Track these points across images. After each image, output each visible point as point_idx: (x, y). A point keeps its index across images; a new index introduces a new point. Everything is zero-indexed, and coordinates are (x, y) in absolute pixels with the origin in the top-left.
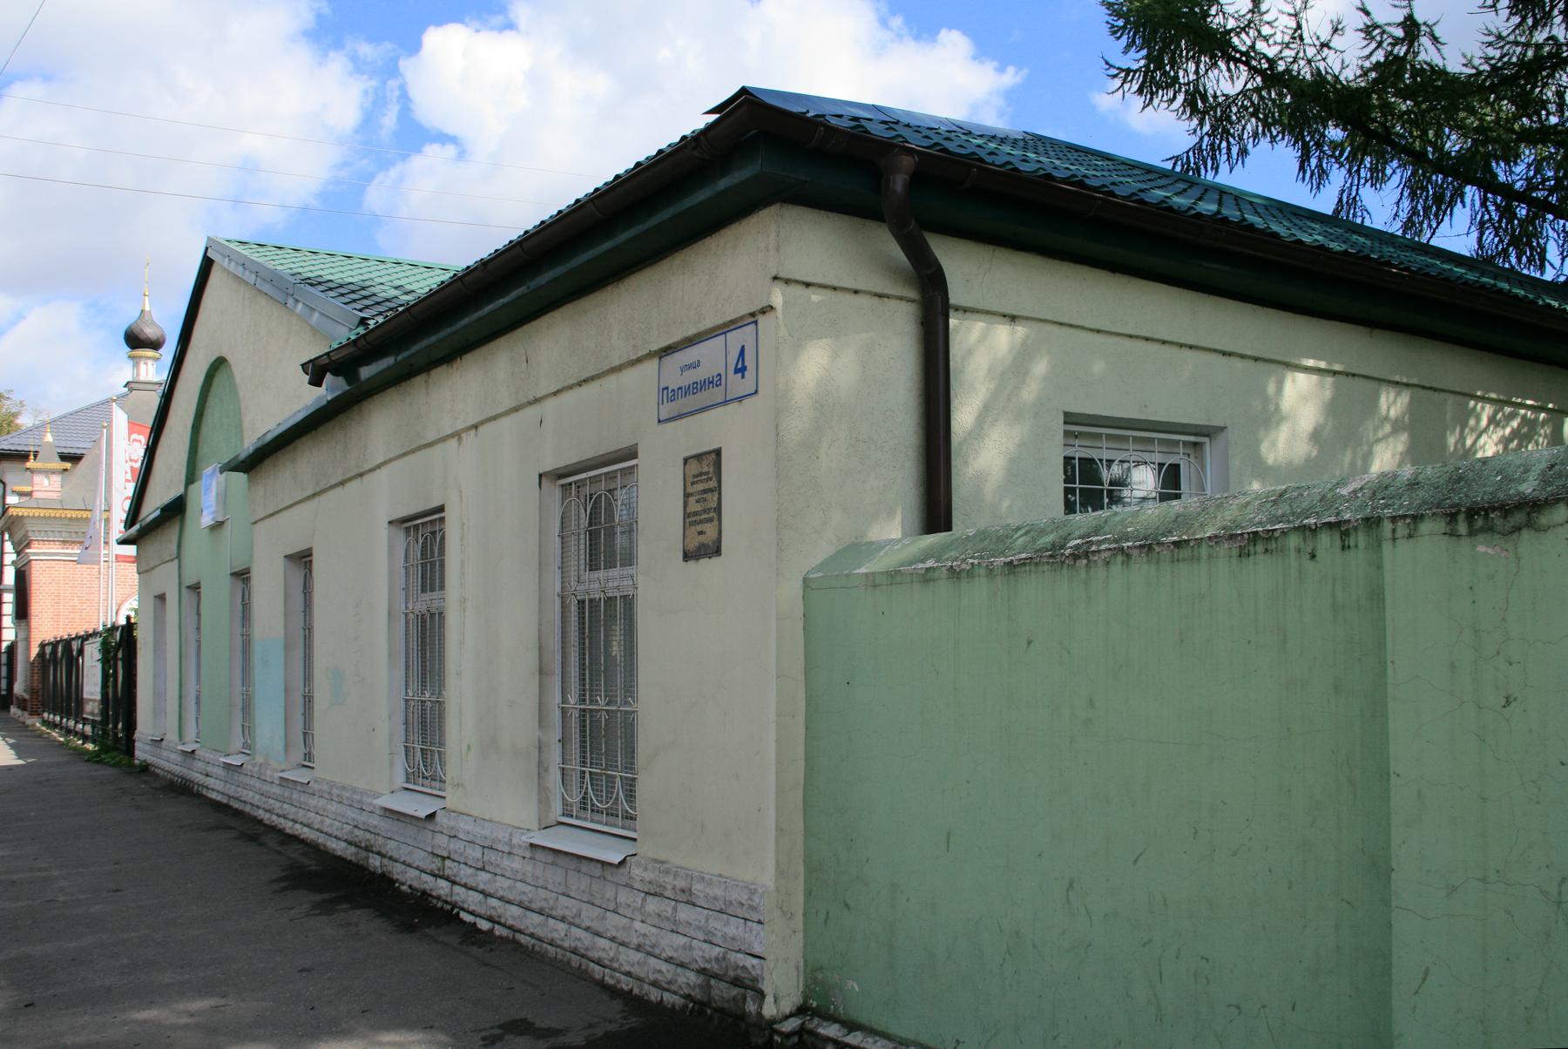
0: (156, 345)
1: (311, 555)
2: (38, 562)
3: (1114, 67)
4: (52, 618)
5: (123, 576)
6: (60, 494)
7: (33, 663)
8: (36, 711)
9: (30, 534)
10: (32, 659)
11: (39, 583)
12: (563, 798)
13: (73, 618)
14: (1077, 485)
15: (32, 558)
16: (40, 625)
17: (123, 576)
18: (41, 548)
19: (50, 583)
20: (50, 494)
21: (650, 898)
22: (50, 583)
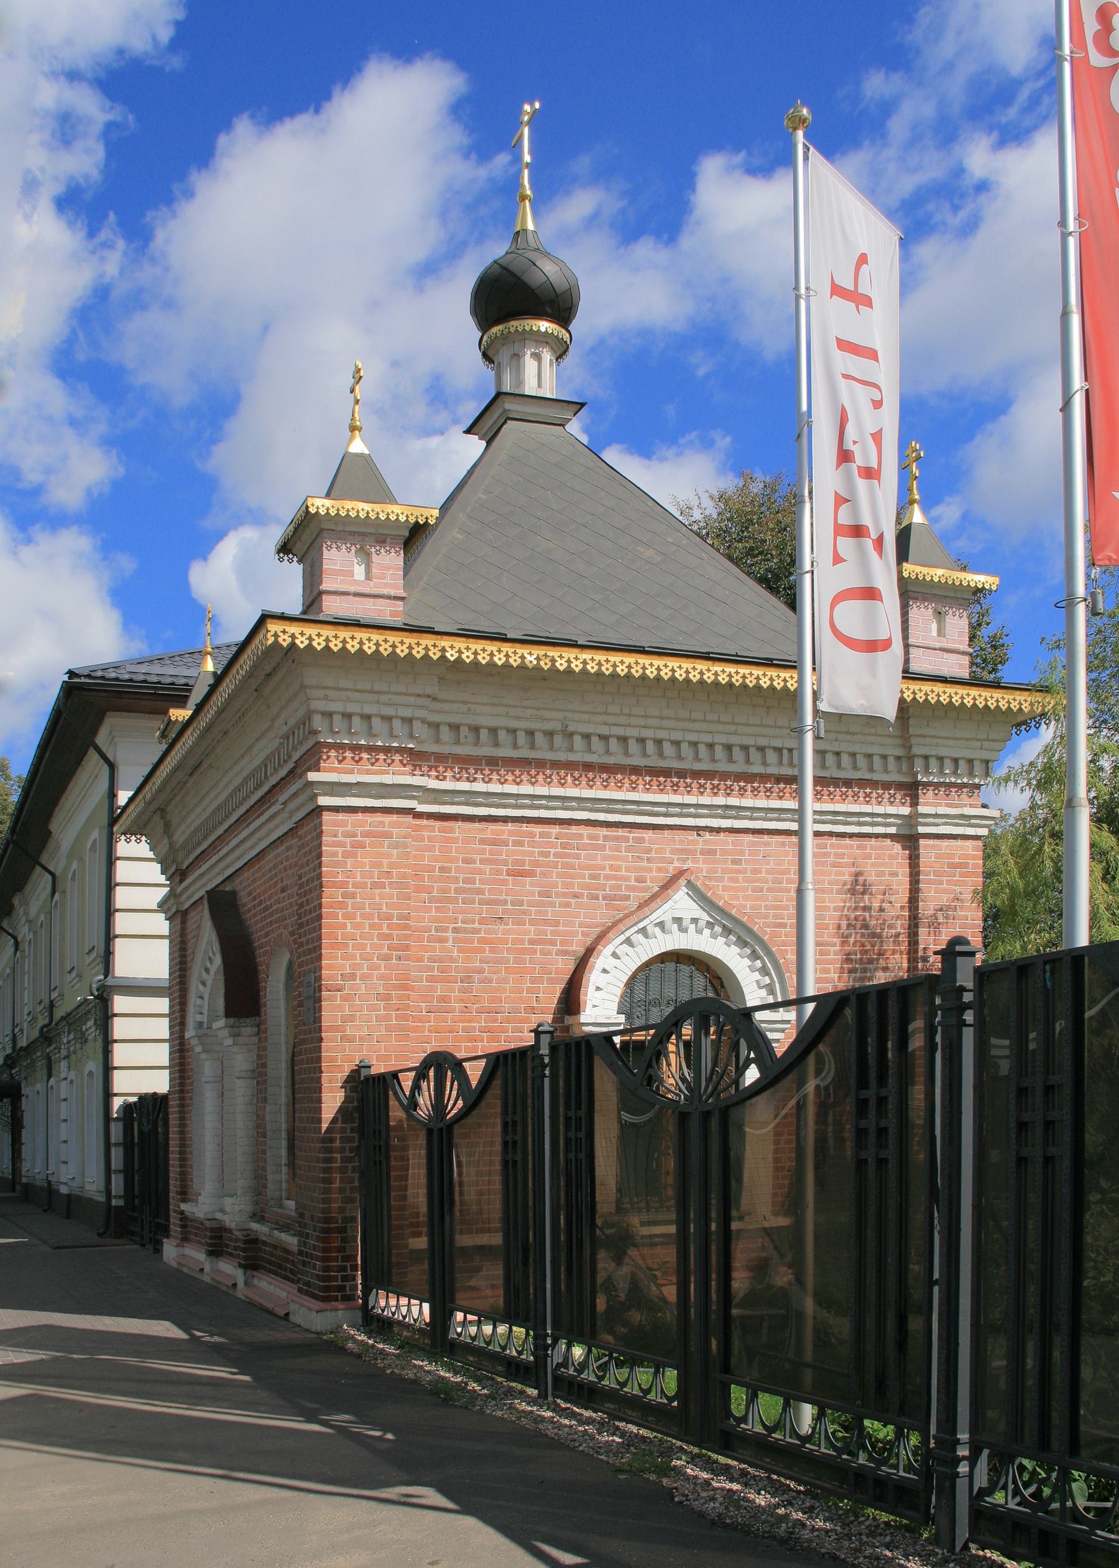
0: (886, 644)
1: (190, 691)
2: (341, 816)
3: (461, 1407)
4: (388, 997)
5: (827, 855)
6: (399, 606)
7: (328, 1139)
8: (342, 1288)
9: (318, 722)
10: (325, 1126)
11: (344, 884)
12: (651, 1058)
13: (443, 999)
14: (376, 921)
15: (323, 801)
16: (345, 1019)
17: (588, 867)
18: (351, 772)
19: (375, 885)
20: (370, 604)
21: (911, 641)
22: (375, 885)
